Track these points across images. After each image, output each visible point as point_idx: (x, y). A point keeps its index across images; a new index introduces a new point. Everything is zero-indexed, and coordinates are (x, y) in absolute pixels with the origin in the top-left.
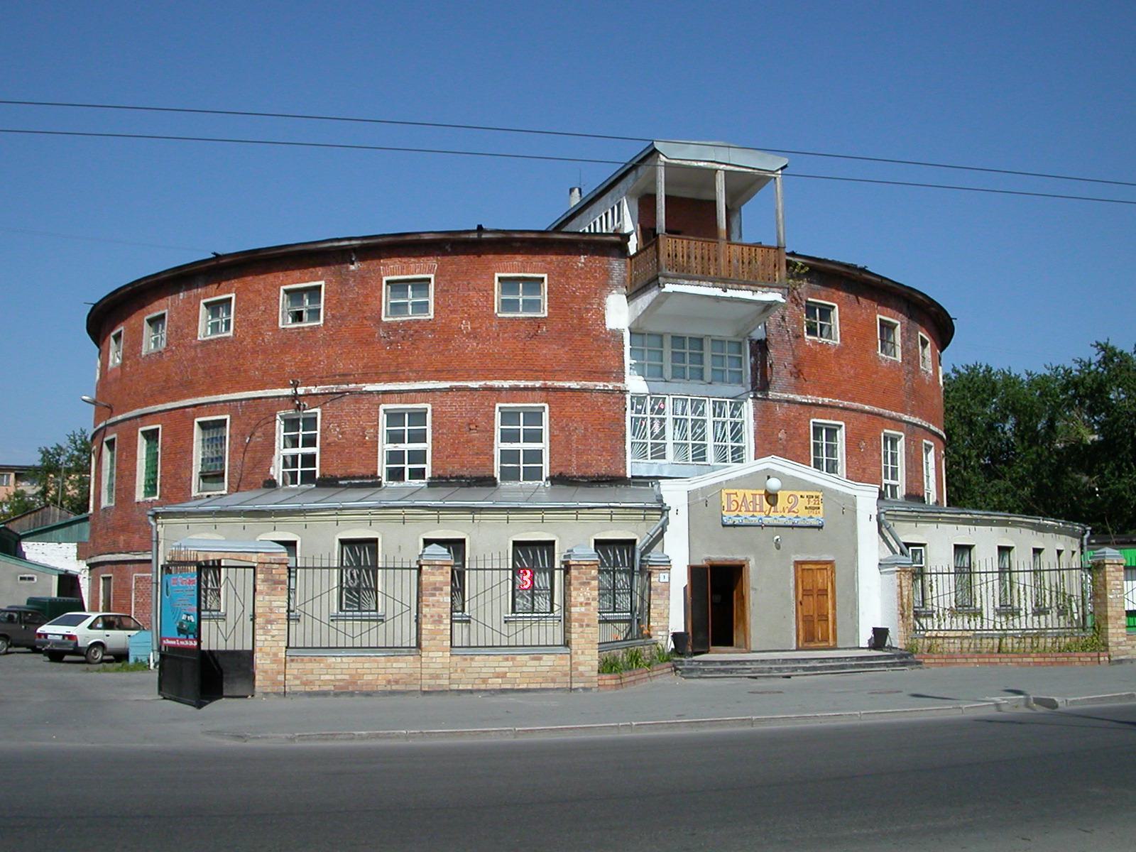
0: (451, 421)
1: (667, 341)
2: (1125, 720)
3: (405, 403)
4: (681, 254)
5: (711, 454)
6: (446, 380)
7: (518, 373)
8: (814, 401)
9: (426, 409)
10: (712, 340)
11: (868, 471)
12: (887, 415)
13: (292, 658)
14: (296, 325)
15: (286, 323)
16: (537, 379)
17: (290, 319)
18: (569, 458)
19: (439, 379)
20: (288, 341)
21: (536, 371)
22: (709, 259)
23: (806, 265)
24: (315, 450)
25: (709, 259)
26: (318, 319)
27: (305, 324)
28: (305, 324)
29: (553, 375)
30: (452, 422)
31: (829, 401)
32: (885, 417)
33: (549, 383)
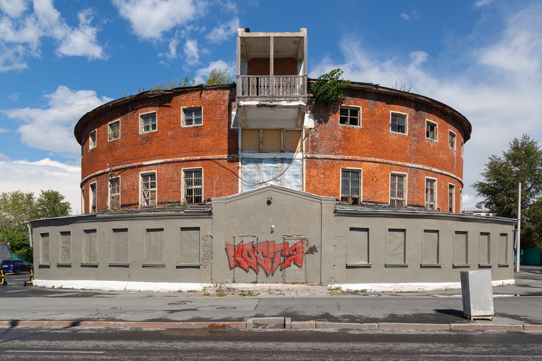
0: (164, 178)
1: (261, 131)
2: (167, 310)
3: (147, 171)
4: (263, 85)
5: (183, 196)
6: (162, 159)
7: (191, 153)
8: (342, 158)
9: (155, 172)
10: (285, 131)
11: (378, 193)
12: (394, 163)
13: (205, 267)
14: (147, 132)
15: (183, 125)
16: (199, 155)
17: (143, 129)
18: (212, 191)
19: (159, 159)
20: (148, 138)
21: (198, 152)
22: (264, 86)
23: (317, 83)
24: (156, 189)
25: (264, 86)
26: (155, 129)
27: (194, 125)
28: (194, 125)
29: (205, 153)
30: (164, 178)
31: (352, 158)
32: (393, 165)
33: (203, 157)
